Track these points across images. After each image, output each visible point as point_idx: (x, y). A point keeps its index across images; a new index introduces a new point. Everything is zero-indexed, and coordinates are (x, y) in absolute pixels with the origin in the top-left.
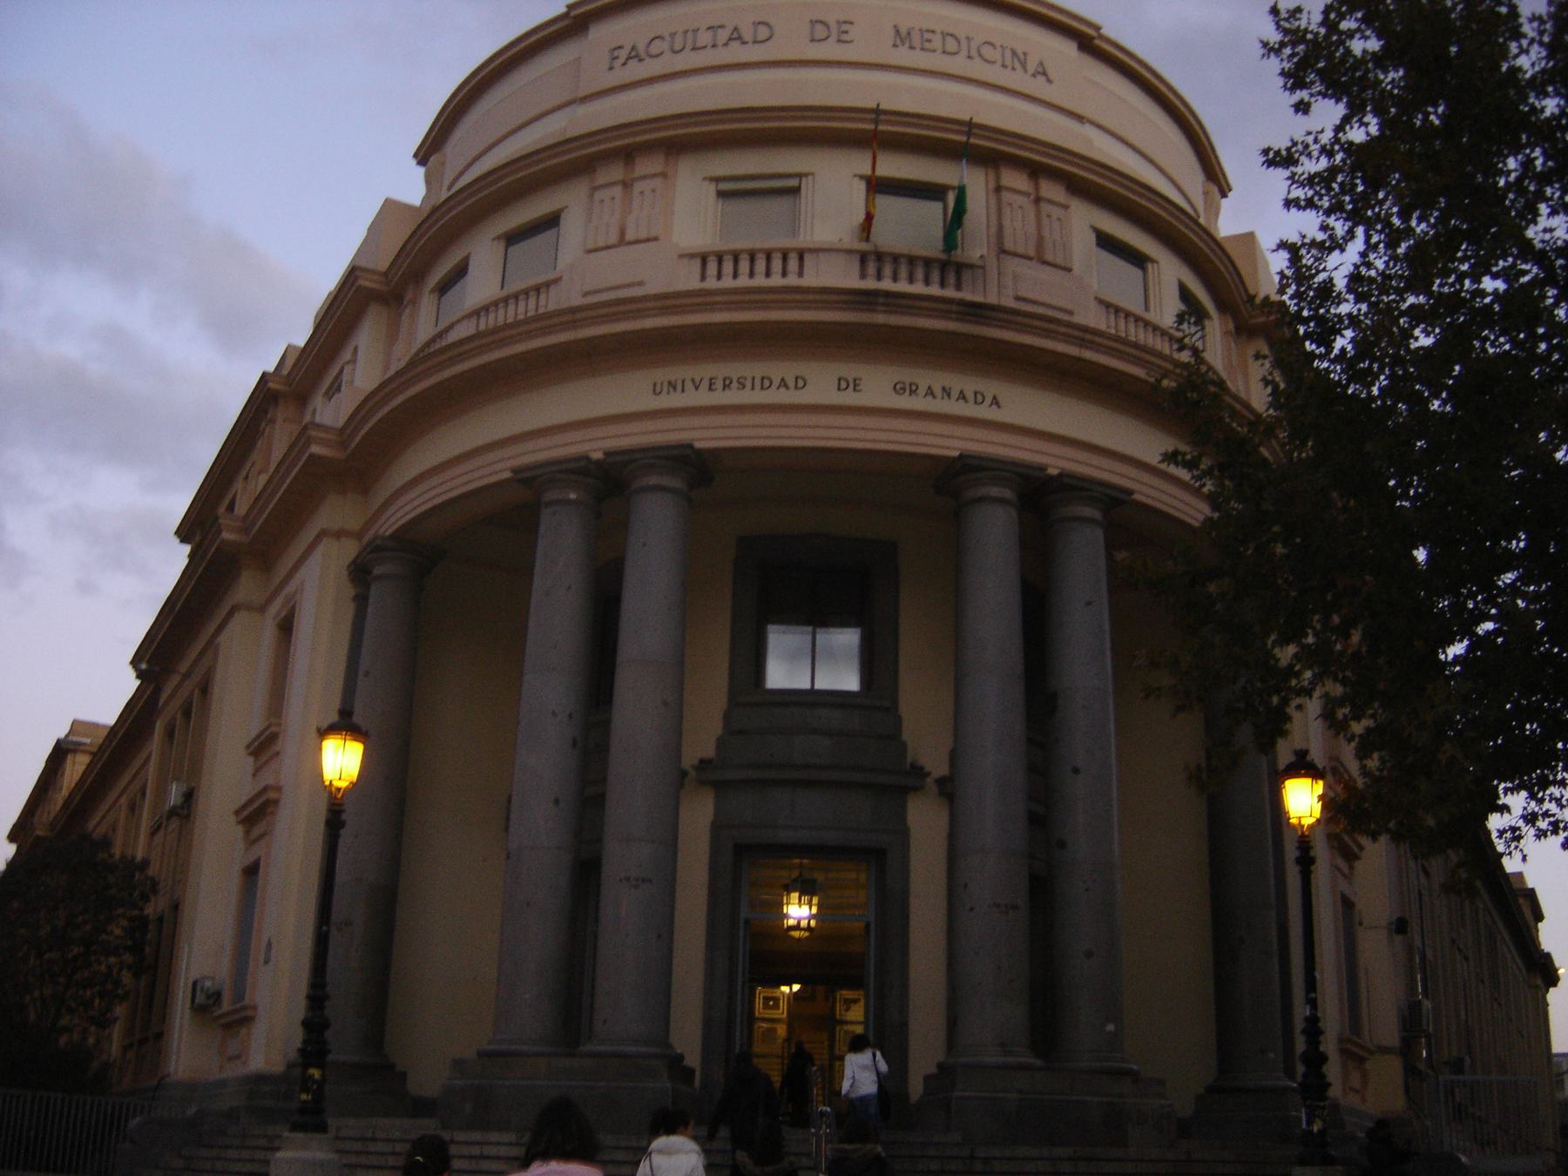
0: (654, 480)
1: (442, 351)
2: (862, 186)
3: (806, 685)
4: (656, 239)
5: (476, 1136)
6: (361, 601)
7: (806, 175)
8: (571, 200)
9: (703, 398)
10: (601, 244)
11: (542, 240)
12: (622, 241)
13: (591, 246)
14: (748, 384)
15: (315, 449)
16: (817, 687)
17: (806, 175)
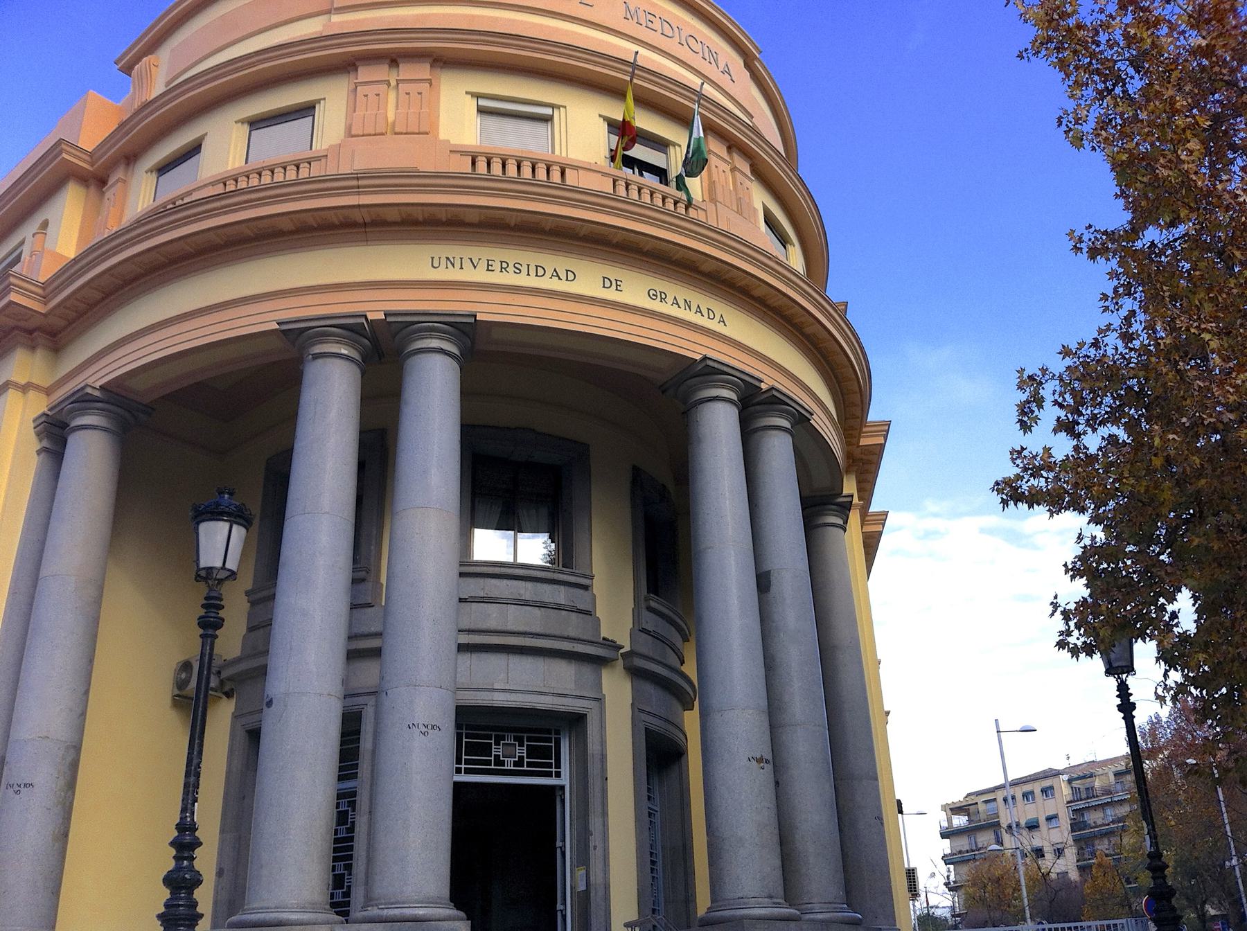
0: (435, 343)
3: (511, 560)
7: (559, 107)
9: (481, 276)
14: (524, 269)
15: (13, 297)
16: (226, 526)
17: (559, 107)
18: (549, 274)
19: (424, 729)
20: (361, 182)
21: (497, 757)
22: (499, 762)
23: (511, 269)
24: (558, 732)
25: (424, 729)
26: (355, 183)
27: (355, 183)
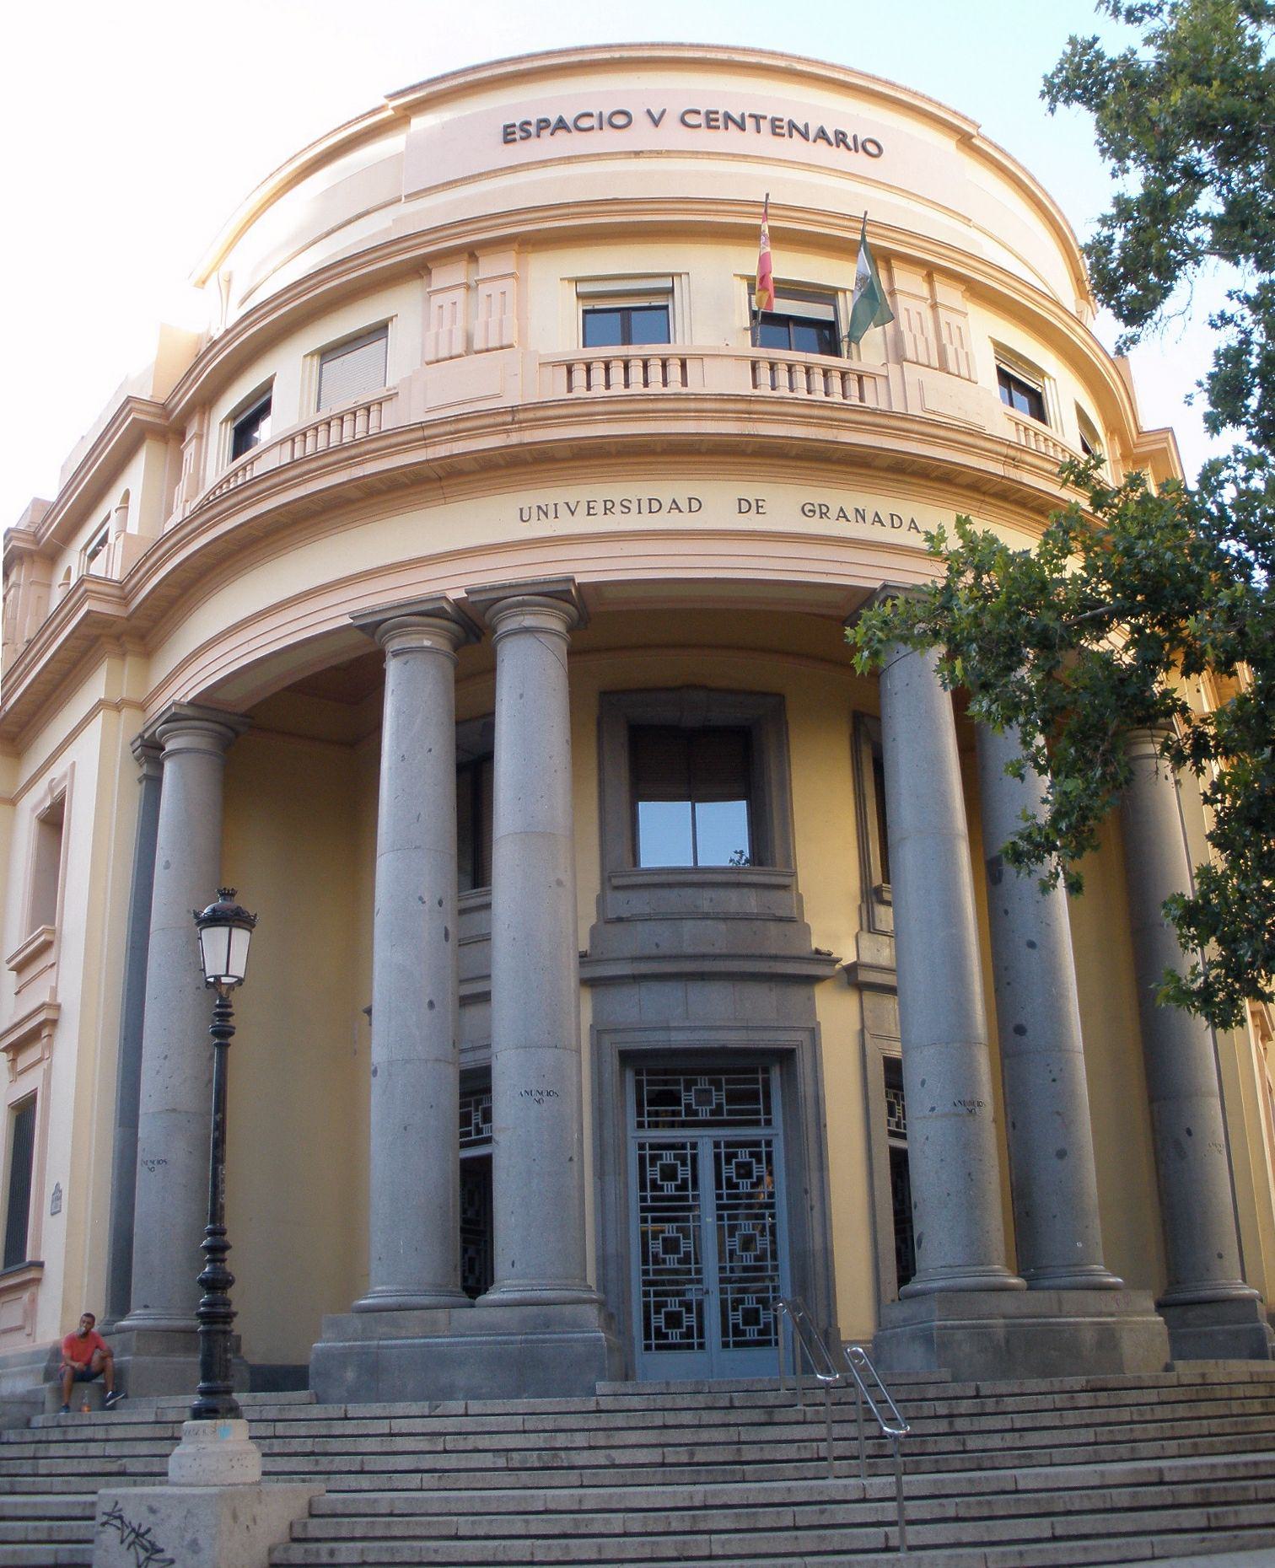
0: (529, 621)
1: (256, 481)
2: (744, 285)
4: (511, 346)
5: (376, 1409)
6: (153, 783)
8: (401, 305)
9: (581, 524)
10: (443, 354)
11: (375, 348)
12: (469, 350)
13: (432, 358)
14: (634, 507)
16: (226, 930)
17: (680, 275)
18: (666, 507)
19: (538, 1097)
20: (427, 432)
21: (688, 1106)
22: (690, 1111)
23: (618, 508)
24: (766, 1071)
25: (538, 1097)
26: (419, 434)
27: (419, 434)
